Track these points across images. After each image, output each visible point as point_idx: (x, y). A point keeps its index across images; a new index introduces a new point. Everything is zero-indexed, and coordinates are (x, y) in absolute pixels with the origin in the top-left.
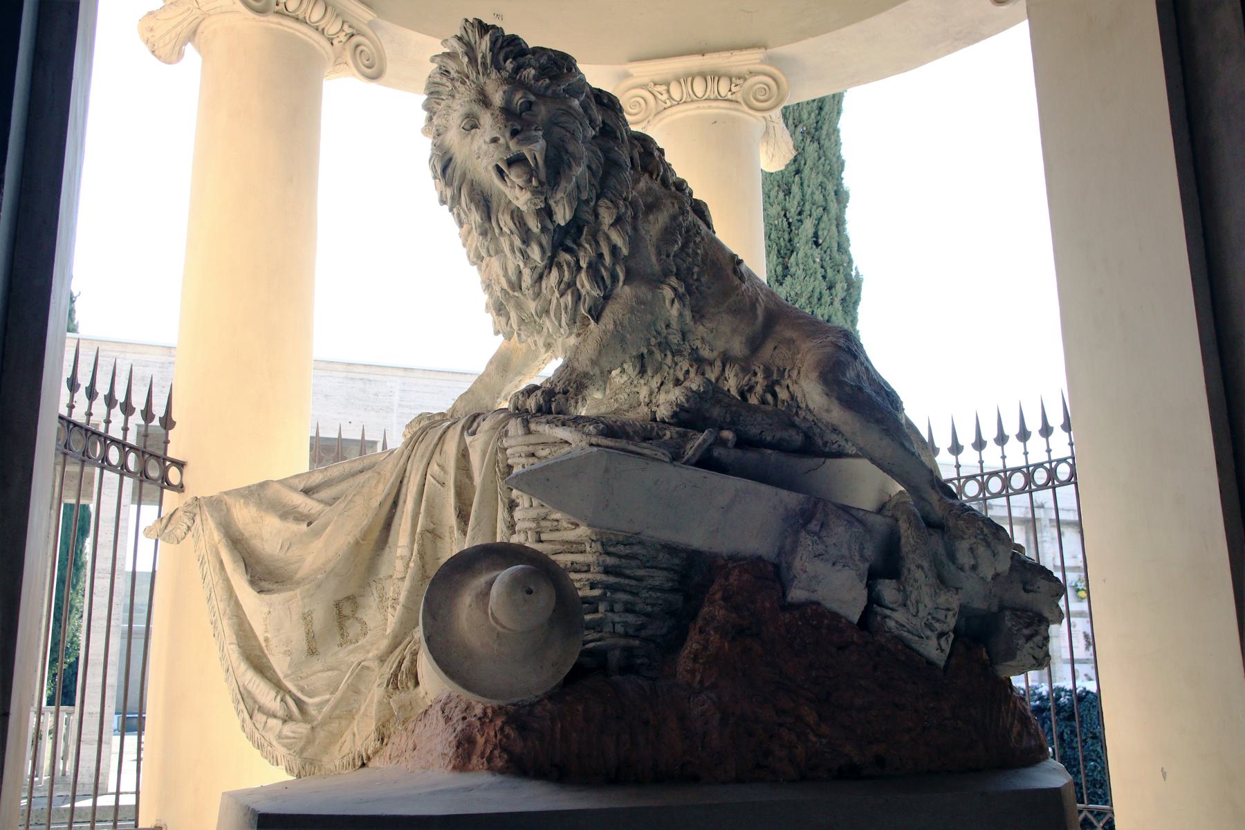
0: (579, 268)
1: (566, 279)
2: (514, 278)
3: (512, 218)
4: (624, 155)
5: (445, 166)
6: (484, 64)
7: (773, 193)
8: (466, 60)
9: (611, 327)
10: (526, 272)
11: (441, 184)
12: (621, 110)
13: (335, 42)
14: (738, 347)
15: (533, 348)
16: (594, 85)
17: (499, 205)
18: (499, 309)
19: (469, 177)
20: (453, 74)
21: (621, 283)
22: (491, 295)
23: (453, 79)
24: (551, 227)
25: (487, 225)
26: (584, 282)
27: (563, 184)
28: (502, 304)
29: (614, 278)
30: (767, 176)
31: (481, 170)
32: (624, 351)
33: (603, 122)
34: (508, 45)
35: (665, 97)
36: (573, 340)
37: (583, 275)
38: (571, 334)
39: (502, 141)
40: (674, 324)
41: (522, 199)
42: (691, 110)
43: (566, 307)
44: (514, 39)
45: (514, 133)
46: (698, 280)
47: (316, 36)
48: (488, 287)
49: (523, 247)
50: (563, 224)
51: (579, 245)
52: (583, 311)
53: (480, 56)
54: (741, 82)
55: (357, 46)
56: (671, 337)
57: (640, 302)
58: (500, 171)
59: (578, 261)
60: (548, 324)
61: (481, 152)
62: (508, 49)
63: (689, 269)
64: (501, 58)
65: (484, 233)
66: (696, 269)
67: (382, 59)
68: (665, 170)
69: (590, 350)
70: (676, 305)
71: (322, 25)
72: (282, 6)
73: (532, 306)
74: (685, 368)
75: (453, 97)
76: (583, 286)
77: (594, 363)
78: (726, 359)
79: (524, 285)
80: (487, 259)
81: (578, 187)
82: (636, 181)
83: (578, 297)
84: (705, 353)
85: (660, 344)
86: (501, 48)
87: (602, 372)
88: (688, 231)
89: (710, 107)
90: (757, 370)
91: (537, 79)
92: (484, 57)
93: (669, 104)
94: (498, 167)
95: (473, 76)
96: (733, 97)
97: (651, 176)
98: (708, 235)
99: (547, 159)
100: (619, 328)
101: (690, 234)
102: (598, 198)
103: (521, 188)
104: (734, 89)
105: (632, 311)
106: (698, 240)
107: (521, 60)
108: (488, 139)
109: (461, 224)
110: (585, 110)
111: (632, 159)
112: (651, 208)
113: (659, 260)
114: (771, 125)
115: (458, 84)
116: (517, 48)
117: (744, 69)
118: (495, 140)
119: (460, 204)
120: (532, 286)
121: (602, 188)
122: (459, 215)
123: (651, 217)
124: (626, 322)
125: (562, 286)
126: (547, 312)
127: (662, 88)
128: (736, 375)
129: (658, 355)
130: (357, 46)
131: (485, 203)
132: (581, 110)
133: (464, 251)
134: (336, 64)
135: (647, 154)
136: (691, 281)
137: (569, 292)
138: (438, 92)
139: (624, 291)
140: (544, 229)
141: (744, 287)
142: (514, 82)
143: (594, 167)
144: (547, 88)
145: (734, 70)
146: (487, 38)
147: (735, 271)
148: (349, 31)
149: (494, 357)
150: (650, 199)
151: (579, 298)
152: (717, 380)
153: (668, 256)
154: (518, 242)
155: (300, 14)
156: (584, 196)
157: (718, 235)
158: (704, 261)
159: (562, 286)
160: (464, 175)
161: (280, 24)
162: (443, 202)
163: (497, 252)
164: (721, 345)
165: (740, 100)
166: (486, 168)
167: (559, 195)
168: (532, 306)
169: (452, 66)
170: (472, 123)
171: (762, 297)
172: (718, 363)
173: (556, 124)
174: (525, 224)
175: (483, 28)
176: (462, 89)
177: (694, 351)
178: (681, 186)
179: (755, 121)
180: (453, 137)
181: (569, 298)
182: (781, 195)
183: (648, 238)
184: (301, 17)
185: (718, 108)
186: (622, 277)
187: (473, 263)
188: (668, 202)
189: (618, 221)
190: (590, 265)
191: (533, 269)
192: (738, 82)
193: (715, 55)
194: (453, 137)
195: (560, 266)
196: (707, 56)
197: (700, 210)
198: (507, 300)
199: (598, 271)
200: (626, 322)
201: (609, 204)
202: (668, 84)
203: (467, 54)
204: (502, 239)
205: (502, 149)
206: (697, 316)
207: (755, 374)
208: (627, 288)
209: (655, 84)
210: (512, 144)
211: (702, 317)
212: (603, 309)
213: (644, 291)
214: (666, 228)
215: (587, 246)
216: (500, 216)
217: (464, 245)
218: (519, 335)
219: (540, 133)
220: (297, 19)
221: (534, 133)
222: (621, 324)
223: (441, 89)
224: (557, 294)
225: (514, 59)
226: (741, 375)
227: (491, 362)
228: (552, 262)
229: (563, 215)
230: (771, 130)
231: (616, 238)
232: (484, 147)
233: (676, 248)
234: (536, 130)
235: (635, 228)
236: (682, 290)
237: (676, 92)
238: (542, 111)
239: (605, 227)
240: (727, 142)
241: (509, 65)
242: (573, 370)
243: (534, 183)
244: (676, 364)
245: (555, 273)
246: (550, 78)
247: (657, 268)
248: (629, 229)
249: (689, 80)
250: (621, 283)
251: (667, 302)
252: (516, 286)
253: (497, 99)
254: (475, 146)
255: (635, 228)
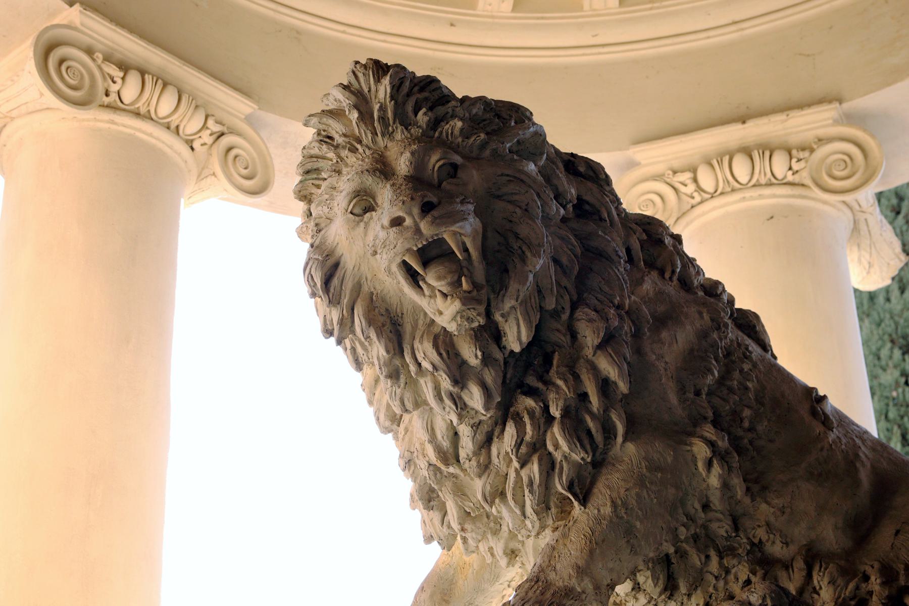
0: (550, 419)
1: (528, 438)
2: (446, 444)
3: (436, 346)
4: (615, 244)
5: (328, 274)
6: (383, 119)
7: (885, 353)
8: (355, 115)
9: (607, 510)
10: (465, 431)
11: (322, 302)
12: (607, 180)
13: (196, 145)
14: (831, 535)
15: (489, 559)
16: (565, 147)
17: (415, 327)
18: (428, 498)
19: (365, 288)
20: (339, 140)
21: (620, 439)
22: (414, 477)
23: (337, 147)
24: (499, 355)
25: (397, 362)
26: (559, 442)
27: (513, 286)
28: (432, 490)
29: (609, 431)
30: (868, 302)
31: (383, 276)
32: (634, 551)
33: (579, 198)
34: (422, 90)
35: (691, 188)
36: (548, 537)
37: (556, 429)
38: (543, 528)
39: (408, 222)
40: (716, 500)
41: (443, 310)
42: (731, 204)
43: (531, 483)
44: (430, 83)
45: (427, 208)
46: (751, 429)
47: (167, 137)
48: (408, 464)
49: (455, 390)
50: (517, 349)
51: (548, 383)
52: (559, 488)
53: (376, 107)
54: (806, 154)
55: (229, 149)
56: (714, 526)
57: (654, 467)
58: (413, 277)
59: (546, 409)
60: (506, 513)
61: (377, 250)
62: (417, 96)
63: (736, 415)
64: (410, 108)
65: (394, 375)
66: (747, 413)
67: (267, 167)
68: (684, 266)
69: (574, 550)
70: (717, 469)
71: (174, 120)
72: (113, 97)
73: (478, 486)
74: (743, 577)
75: (339, 172)
76: (557, 446)
77: (581, 571)
78: (813, 557)
79: (462, 454)
80: (406, 417)
81: (539, 292)
82: (639, 282)
83: (549, 466)
84: (776, 549)
85: (695, 538)
86: (409, 95)
87: (597, 587)
88: (728, 354)
89: (761, 197)
90: (869, 570)
91: (465, 134)
92: (382, 108)
93: (698, 198)
94: (406, 267)
95: (367, 138)
96: (796, 179)
97: (662, 273)
98: (763, 360)
99: (484, 251)
100: (622, 512)
101: (732, 359)
102: (574, 307)
103: (445, 296)
104: (796, 166)
105: (641, 482)
106: (746, 367)
107: (440, 110)
108: (386, 222)
109: (358, 365)
110: (548, 179)
111: (628, 251)
112: (662, 321)
113: (683, 401)
114: (861, 217)
115: (345, 153)
116: (436, 95)
117: (809, 136)
118: (397, 222)
119: (353, 332)
120: (476, 453)
121: (580, 294)
122: (354, 350)
123: (664, 334)
124: (633, 502)
125: (523, 450)
126: (503, 495)
127: (686, 177)
128: (832, 582)
129: (695, 559)
130: (229, 149)
131: (392, 327)
132: (540, 178)
133: (371, 411)
134: (200, 177)
135: (654, 243)
136: (740, 433)
137: (535, 459)
138: (317, 170)
139: (628, 452)
140: (487, 360)
141: (832, 436)
142: (429, 139)
143: (564, 260)
144: (483, 146)
145: (794, 140)
146: (386, 81)
147: (814, 413)
148: (217, 128)
149: (426, 581)
150: (661, 308)
151: (553, 467)
152: (801, 591)
153: (698, 393)
154: (446, 384)
155: (141, 106)
156: (550, 304)
157: (782, 362)
158: (759, 401)
159: (523, 450)
160: (358, 288)
161: (113, 122)
162: (328, 333)
163: (417, 405)
164: (800, 533)
165: (808, 182)
166: (389, 271)
167: (509, 303)
168: (478, 486)
169: (336, 128)
170: (364, 204)
171: (864, 451)
172: (799, 564)
173: (499, 197)
174: (457, 354)
175: (379, 68)
176: (352, 159)
177: (757, 546)
178: (713, 289)
179: (831, 210)
180: (339, 232)
181: (535, 467)
182: (897, 353)
183: (661, 365)
184: (143, 110)
185: (774, 196)
186: (620, 428)
187: (386, 430)
188: (693, 310)
189: (608, 342)
190: (566, 413)
191: (476, 426)
192: (802, 155)
193: (763, 121)
194: (339, 232)
195: (518, 420)
196: (750, 124)
197: (749, 324)
198: (439, 482)
199: (581, 422)
200: (633, 502)
201: (593, 314)
202: (694, 171)
203: (356, 107)
204: (422, 381)
205: (409, 234)
206: (756, 488)
207: (866, 578)
208: (631, 447)
209: (675, 172)
210: (424, 226)
211: (765, 488)
212: (593, 483)
213: (661, 451)
214: (691, 351)
215: (560, 383)
216: (417, 344)
217: (370, 402)
218: (465, 540)
219: (471, 207)
220: (137, 114)
221: (459, 207)
222: (625, 504)
223: (321, 164)
224: (516, 464)
225: (431, 109)
226: (840, 581)
227: (422, 589)
228: (505, 412)
229: (516, 335)
230: (863, 226)
231: (608, 368)
232: (382, 234)
233: (709, 380)
234: (462, 202)
235: (638, 351)
236: (723, 443)
237: (706, 180)
238: (474, 177)
239: (589, 352)
240: (798, 246)
241: (422, 118)
242: (548, 584)
243: (465, 285)
244: (728, 572)
245: (510, 430)
246: (487, 134)
247: (680, 412)
248: (628, 352)
249: (726, 159)
250: (620, 439)
251: (700, 465)
252: (450, 456)
253: (403, 164)
254: (370, 237)
255: (638, 351)
